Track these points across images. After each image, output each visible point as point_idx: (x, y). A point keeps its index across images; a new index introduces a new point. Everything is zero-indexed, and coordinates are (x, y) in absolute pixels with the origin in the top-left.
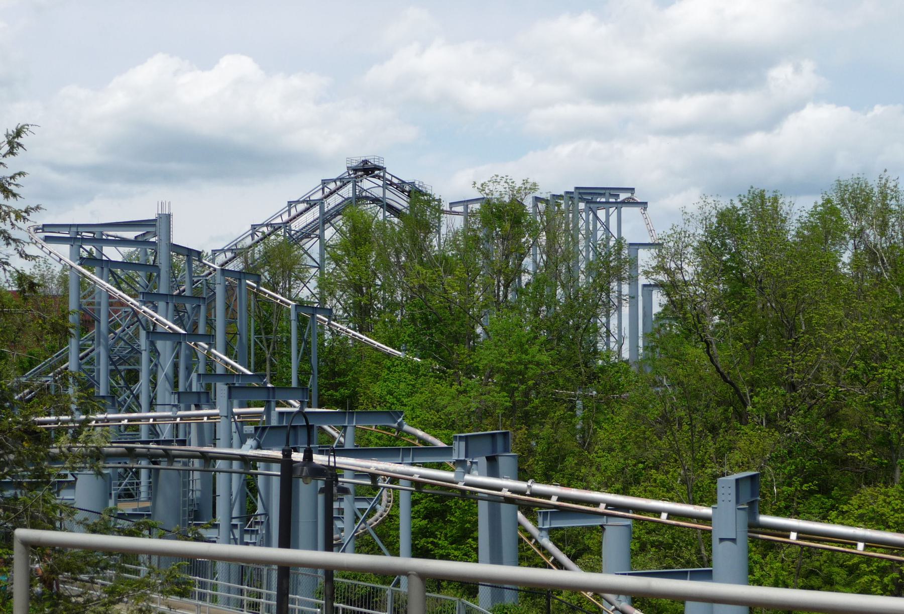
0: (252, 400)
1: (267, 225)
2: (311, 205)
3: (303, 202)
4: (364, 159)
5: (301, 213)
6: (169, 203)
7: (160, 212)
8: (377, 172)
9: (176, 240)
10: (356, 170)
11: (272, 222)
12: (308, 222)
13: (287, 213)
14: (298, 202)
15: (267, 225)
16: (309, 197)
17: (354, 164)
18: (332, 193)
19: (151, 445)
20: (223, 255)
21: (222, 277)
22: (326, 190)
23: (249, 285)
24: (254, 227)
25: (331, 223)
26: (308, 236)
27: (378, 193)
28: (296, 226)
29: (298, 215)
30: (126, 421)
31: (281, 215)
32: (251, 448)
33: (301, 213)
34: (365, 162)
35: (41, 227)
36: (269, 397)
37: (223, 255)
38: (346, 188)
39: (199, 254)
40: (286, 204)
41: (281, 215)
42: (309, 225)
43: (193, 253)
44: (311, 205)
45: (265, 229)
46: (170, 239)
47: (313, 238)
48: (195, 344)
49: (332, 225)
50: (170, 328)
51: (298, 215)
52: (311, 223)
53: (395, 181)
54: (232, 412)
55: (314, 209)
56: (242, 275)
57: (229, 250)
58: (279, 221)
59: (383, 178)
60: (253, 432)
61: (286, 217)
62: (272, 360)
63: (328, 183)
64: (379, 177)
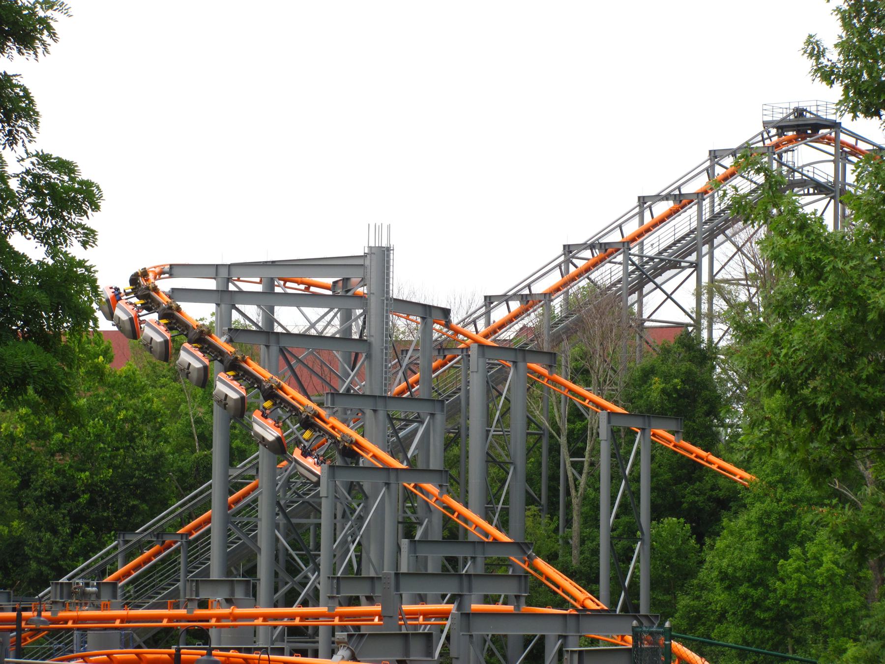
0: (430, 593)
1: (592, 247)
2: (681, 201)
3: (667, 198)
4: (795, 105)
5: (662, 220)
6: (389, 227)
7: (372, 244)
8: (822, 131)
9: (395, 293)
10: (782, 128)
11: (603, 241)
12: (679, 235)
13: (636, 220)
14: (659, 198)
15: (592, 247)
16: (679, 188)
17: (778, 117)
18: (579, 275)
19: (231, 653)
20: (504, 306)
21: (481, 360)
22: (648, 219)
23: (534, 372)
24: (569, 250)
25: (726, 236)
26: (674, 264)
27: (825, 173)
28: (654, 244)
29: (655, 225)
30: (261, 619)
31: (620, 226)
32: (343, 658)
33: (662, 220)
34: (800, 112)
35: (167, 268)
36: (461, 589)
37: (504, 306)
38: (684, 215)
39: (446, 312)
40: (635, 202)
41: (620, 226)
42: (679, 241)
43: (434, 311)
44: (681, 201)
45: (587, 254)
46: (388, 293)
47: (684, 268)
48: (415, 487)
49: (728, 238)
50: (375, 456)
51: (655, 225)
52: (683, 238)
53: (862, 146)
54: (401, 609)
55: (689, 212)
56: (520, 356)
57: (515, 297)
58: (615, 237)
59: (833, 142)
60: (346, 640)
61: (632, 228)
62: (44, 631)
63: (722, 157)
64: (829, 141)
